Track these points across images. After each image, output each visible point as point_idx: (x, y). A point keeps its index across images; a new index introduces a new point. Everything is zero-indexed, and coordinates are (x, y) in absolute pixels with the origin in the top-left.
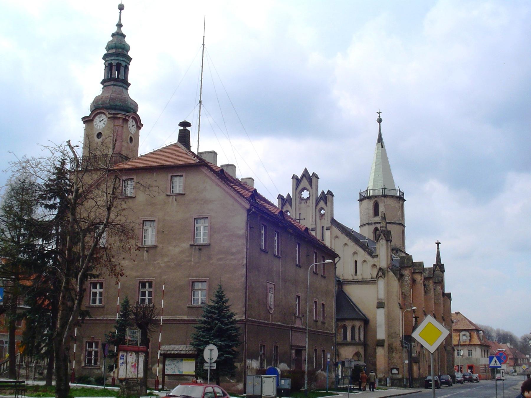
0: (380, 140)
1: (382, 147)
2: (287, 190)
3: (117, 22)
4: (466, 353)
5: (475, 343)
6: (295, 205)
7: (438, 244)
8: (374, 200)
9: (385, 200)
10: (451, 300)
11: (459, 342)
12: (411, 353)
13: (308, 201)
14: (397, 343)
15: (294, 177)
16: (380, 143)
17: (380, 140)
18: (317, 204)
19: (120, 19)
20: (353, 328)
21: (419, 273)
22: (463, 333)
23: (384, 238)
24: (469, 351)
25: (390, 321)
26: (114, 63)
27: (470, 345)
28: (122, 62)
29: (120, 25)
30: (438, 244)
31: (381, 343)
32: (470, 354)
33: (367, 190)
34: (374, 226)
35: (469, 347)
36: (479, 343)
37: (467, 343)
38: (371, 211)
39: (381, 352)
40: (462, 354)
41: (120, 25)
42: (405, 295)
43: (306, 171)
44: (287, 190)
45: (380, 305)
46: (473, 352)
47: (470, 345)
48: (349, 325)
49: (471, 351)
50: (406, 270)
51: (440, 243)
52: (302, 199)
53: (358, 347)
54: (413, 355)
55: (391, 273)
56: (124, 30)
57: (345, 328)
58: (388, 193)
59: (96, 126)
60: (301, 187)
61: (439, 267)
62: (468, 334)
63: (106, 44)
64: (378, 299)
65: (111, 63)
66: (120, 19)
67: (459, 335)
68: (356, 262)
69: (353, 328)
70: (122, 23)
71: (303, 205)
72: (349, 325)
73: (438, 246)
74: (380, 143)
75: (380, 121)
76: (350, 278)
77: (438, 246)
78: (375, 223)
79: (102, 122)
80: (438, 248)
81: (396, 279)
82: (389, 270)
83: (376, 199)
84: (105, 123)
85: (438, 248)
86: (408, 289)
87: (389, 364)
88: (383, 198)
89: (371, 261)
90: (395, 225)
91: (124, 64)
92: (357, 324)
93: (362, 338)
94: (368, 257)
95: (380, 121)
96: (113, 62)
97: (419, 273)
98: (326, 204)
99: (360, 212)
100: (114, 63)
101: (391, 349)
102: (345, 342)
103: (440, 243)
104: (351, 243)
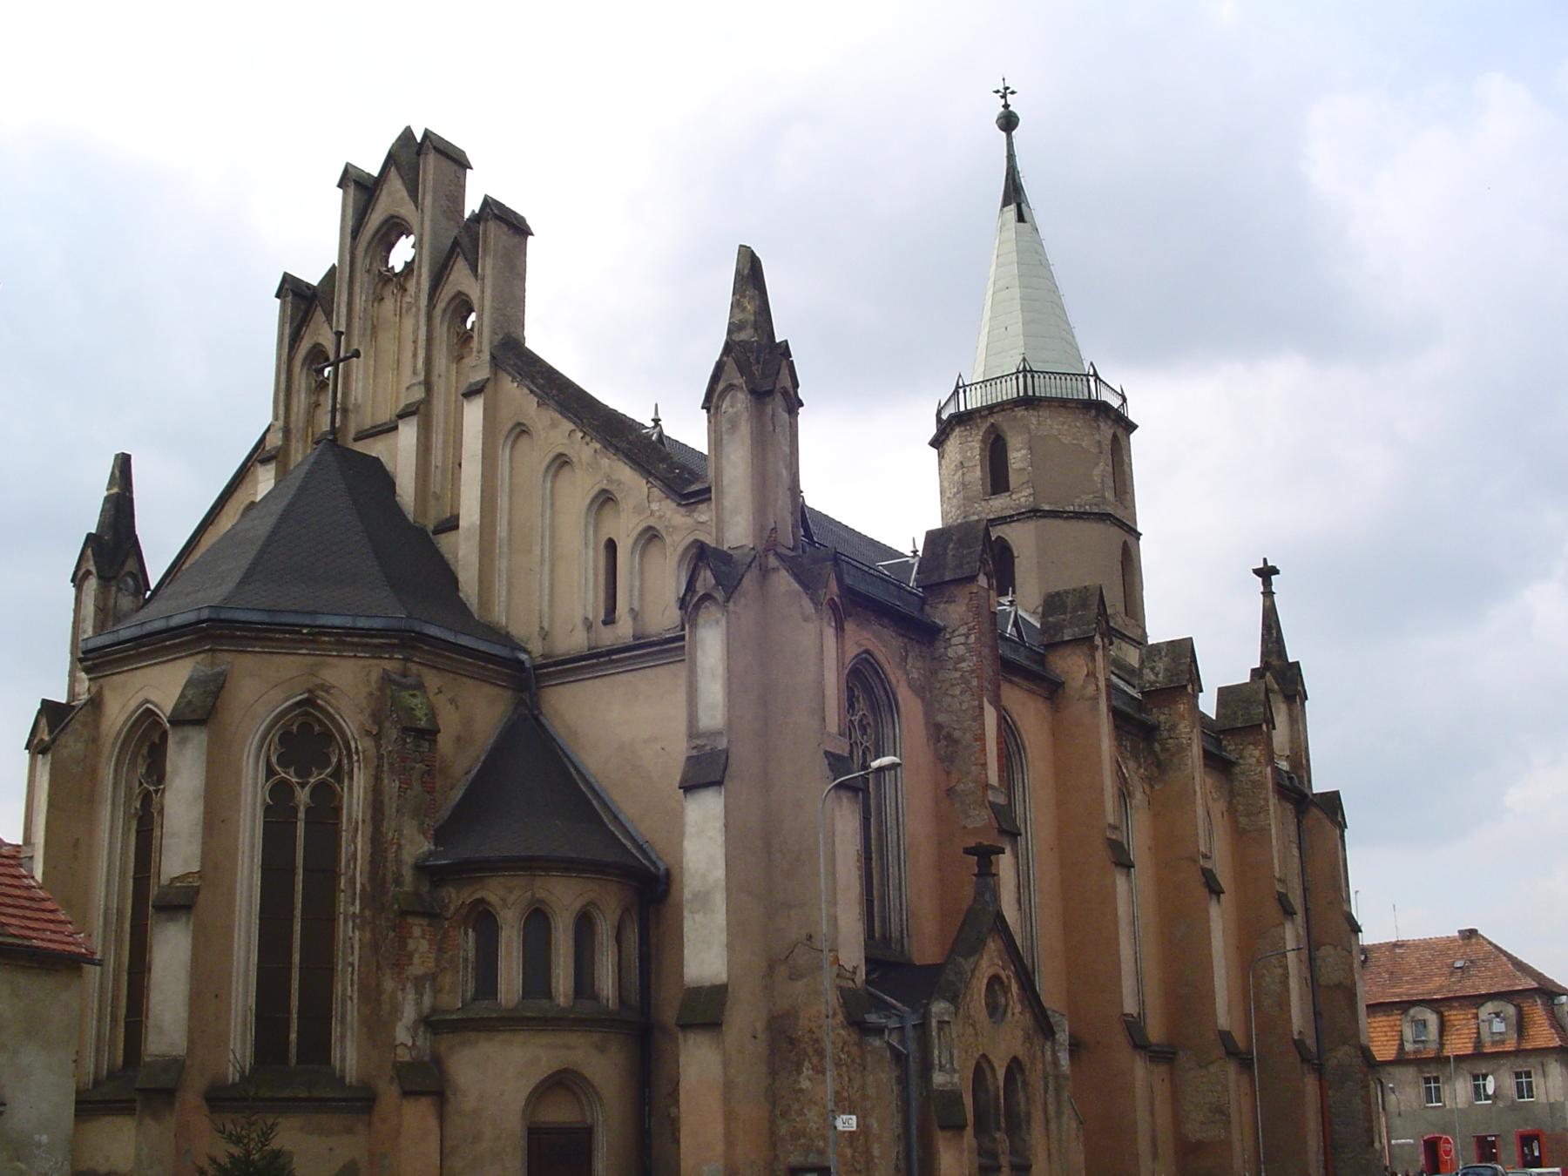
0: (1014, 193)
1: (1021, 218)
4: (1509, 1083)
5: (1540, 1043)
6: (344, 310)
7: (1266, 573)
8: (985, 426)
9: (1032, 418)
10: (1342, 826)
11: (1478, 1042)
12: (926, 1069)
14: (821, 1007)
15: (351, 179)
16: (1013, 206)
17: (1014, 193)
20: (537, 921)
21: (1076, 642)
22: (1490, 1007)
23: (739, 380)
24: (1518, 1075)
25: (763, 859)
27: (1518, 1053)
30: (1266, 573)
31: (707, 1010)
32: (1524, 1090)
33: (956, 392)
35: (1519, 1061)
36: (1557, 1042)
37: (1510, 1046)
39: (699, 1066)
40: (1490, 1091)
42: (949, 737)
45: (705, 771)
46: (1536, 1080)
47: (1518, 1053)
48: (507, 901)
49: (1528, 1075)
50: (951, 601)
51: (1275, 571)
53: (573, 1039)
54: (938, 1078)
55: (784, 582)
57: (484, 921)
58: (1044, 388)
61: (1279, 677)
62: (1510, 1010)
64: (693, 733)
67: (1476, 1016)
68: (611, 546)
69: (537, 921)
72: (507, 901)
73: (1267, 583)
74: (1013, 206)
75: (1008, 122)
76: (573, 640)
77: (1267, 583)
80: (1268, 593)
81: (808, 606)
82: (773, 561)
83: (997, 419)
85: (1268, 593)
86: (968, 702)
87: (774, 1141)
88: (1020, 412)
89: (681, 526)
92: (565, 897)
93: (606, 983)
94: (667, 512)
95: (1008, 122)
97: (1076, 642)
98: (474, 269)
99: (942, 492)
101: (784, 1043)
102: (483, 1009)
103: (1275, 571)
104: (584, 450)
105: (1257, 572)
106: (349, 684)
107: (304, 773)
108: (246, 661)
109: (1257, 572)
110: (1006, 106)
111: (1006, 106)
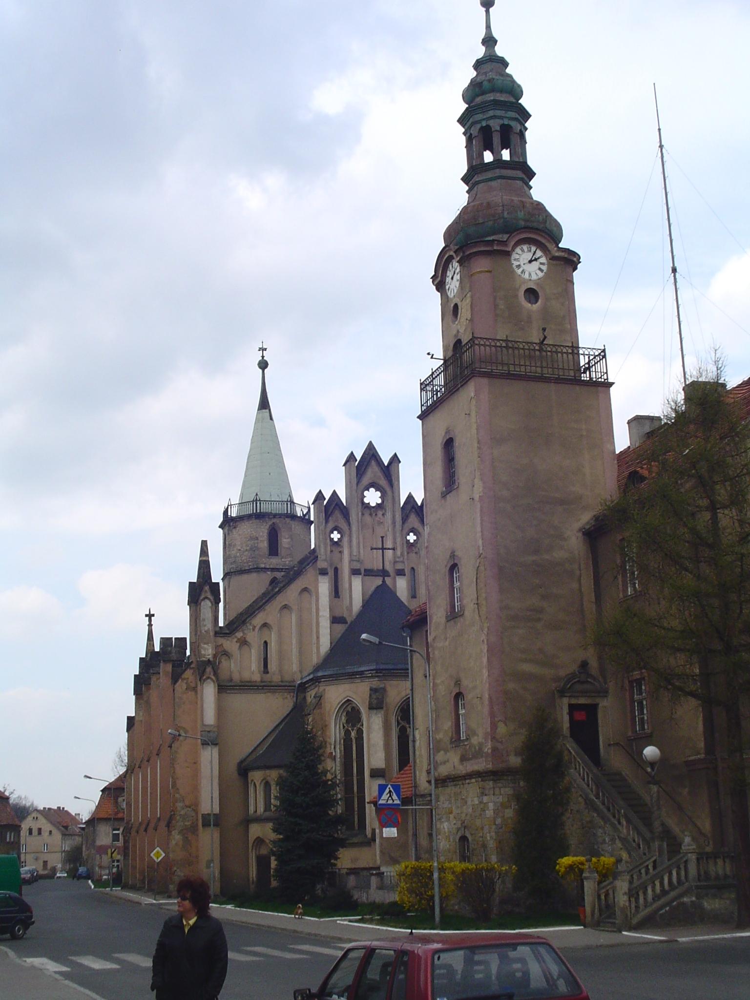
0: (264, 404)
2: (336, 484)
3: (482, 34)
7: (150, 616)
8: (270, 523)
13: (380, 513)
17: (264, 404)
18: (404, 520)
19: (488, 27)
20: (267, 785)
26: (495, 125)
28: (513, 124)
29: (489, 41)
30: (150, 616)
34: (269, 576)
38: (264, 545)
41: (489, 41)
43: (371, 448)
44: (336, 484)
51: (153, 615)
52: (367, 506)
56: (500, 50)
59: (519, 271)
60: (366, 480)
63: (469, 81)
65: (488, 127)
66: (488, 27)
70: (495, 34)
71: (368, 519)
73: (150, 620)
77: (150, 620)
78: (273, 570)
79: (535, 264)
80: (150, 625)
83: (274, 520)
84: (544, 268)
85: (150, 625)
90: (245, 577)
91: (517, 127)
96: (491, 123)
100: (495, 125)
103: (153, 615)
105: (146, 616)
106: (358, 692)
107: (353, 726)
108: (327, 688)
109: (146, 616)
110: (263, 357)
111: (263, 357)
